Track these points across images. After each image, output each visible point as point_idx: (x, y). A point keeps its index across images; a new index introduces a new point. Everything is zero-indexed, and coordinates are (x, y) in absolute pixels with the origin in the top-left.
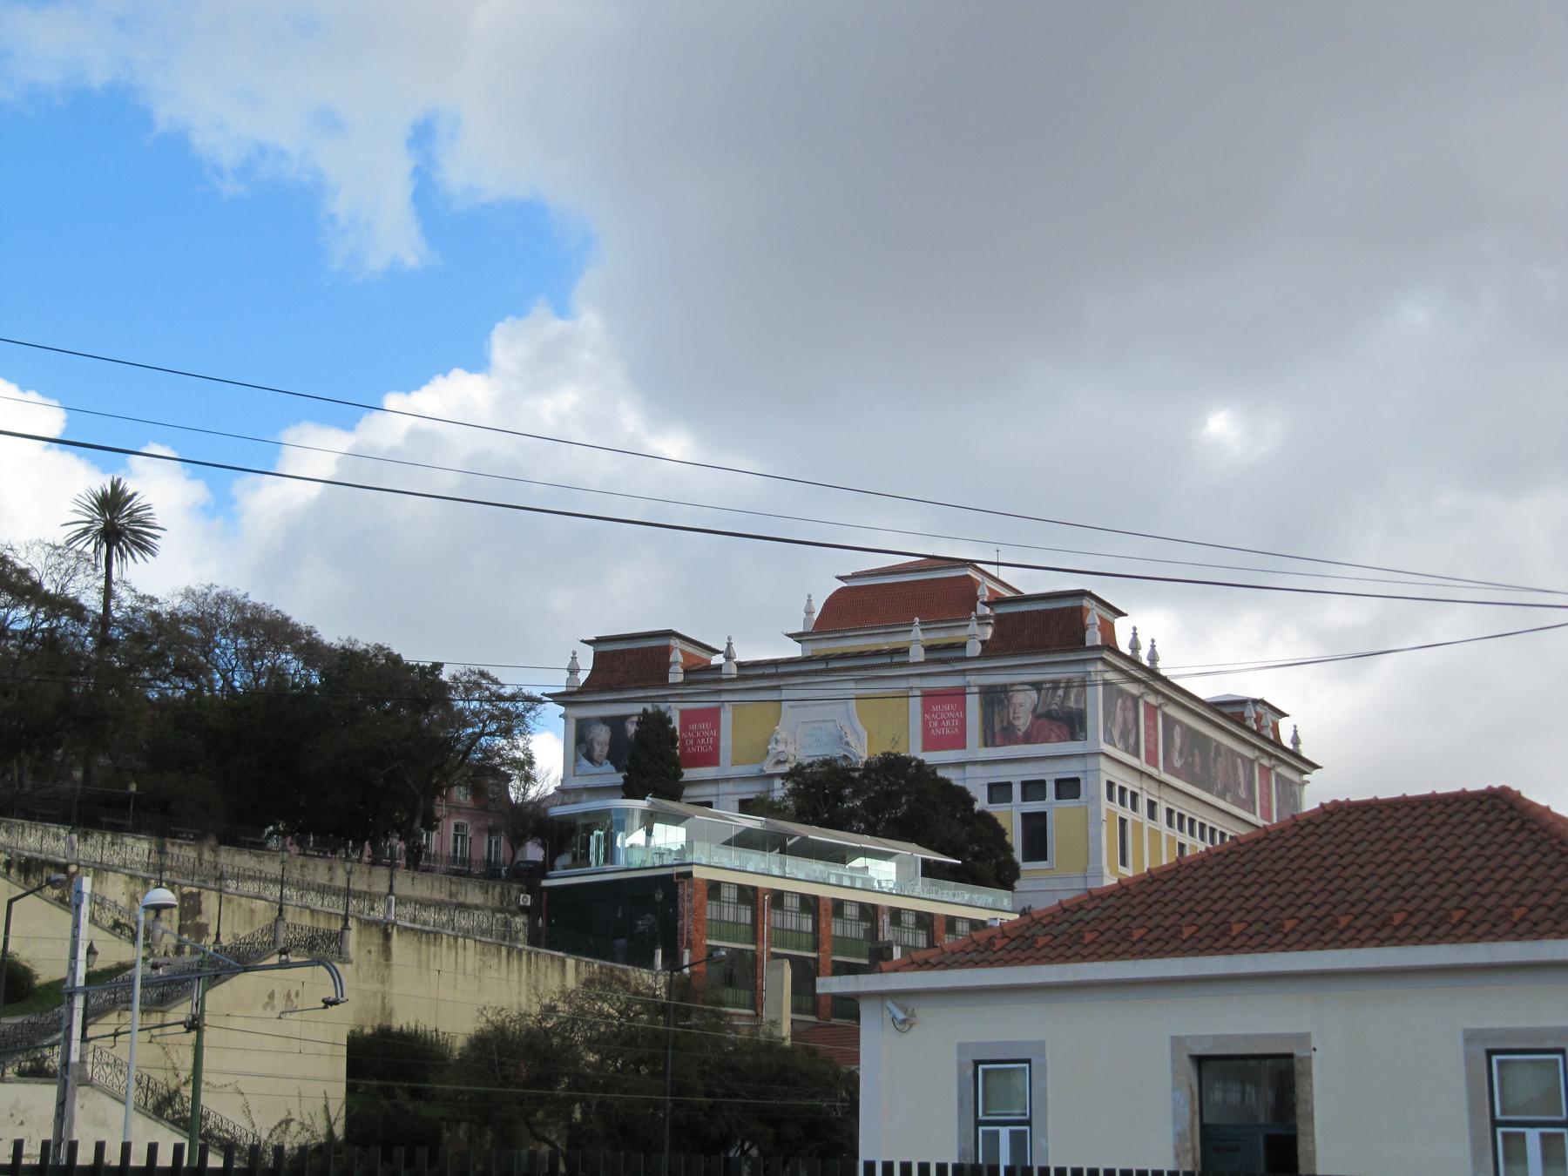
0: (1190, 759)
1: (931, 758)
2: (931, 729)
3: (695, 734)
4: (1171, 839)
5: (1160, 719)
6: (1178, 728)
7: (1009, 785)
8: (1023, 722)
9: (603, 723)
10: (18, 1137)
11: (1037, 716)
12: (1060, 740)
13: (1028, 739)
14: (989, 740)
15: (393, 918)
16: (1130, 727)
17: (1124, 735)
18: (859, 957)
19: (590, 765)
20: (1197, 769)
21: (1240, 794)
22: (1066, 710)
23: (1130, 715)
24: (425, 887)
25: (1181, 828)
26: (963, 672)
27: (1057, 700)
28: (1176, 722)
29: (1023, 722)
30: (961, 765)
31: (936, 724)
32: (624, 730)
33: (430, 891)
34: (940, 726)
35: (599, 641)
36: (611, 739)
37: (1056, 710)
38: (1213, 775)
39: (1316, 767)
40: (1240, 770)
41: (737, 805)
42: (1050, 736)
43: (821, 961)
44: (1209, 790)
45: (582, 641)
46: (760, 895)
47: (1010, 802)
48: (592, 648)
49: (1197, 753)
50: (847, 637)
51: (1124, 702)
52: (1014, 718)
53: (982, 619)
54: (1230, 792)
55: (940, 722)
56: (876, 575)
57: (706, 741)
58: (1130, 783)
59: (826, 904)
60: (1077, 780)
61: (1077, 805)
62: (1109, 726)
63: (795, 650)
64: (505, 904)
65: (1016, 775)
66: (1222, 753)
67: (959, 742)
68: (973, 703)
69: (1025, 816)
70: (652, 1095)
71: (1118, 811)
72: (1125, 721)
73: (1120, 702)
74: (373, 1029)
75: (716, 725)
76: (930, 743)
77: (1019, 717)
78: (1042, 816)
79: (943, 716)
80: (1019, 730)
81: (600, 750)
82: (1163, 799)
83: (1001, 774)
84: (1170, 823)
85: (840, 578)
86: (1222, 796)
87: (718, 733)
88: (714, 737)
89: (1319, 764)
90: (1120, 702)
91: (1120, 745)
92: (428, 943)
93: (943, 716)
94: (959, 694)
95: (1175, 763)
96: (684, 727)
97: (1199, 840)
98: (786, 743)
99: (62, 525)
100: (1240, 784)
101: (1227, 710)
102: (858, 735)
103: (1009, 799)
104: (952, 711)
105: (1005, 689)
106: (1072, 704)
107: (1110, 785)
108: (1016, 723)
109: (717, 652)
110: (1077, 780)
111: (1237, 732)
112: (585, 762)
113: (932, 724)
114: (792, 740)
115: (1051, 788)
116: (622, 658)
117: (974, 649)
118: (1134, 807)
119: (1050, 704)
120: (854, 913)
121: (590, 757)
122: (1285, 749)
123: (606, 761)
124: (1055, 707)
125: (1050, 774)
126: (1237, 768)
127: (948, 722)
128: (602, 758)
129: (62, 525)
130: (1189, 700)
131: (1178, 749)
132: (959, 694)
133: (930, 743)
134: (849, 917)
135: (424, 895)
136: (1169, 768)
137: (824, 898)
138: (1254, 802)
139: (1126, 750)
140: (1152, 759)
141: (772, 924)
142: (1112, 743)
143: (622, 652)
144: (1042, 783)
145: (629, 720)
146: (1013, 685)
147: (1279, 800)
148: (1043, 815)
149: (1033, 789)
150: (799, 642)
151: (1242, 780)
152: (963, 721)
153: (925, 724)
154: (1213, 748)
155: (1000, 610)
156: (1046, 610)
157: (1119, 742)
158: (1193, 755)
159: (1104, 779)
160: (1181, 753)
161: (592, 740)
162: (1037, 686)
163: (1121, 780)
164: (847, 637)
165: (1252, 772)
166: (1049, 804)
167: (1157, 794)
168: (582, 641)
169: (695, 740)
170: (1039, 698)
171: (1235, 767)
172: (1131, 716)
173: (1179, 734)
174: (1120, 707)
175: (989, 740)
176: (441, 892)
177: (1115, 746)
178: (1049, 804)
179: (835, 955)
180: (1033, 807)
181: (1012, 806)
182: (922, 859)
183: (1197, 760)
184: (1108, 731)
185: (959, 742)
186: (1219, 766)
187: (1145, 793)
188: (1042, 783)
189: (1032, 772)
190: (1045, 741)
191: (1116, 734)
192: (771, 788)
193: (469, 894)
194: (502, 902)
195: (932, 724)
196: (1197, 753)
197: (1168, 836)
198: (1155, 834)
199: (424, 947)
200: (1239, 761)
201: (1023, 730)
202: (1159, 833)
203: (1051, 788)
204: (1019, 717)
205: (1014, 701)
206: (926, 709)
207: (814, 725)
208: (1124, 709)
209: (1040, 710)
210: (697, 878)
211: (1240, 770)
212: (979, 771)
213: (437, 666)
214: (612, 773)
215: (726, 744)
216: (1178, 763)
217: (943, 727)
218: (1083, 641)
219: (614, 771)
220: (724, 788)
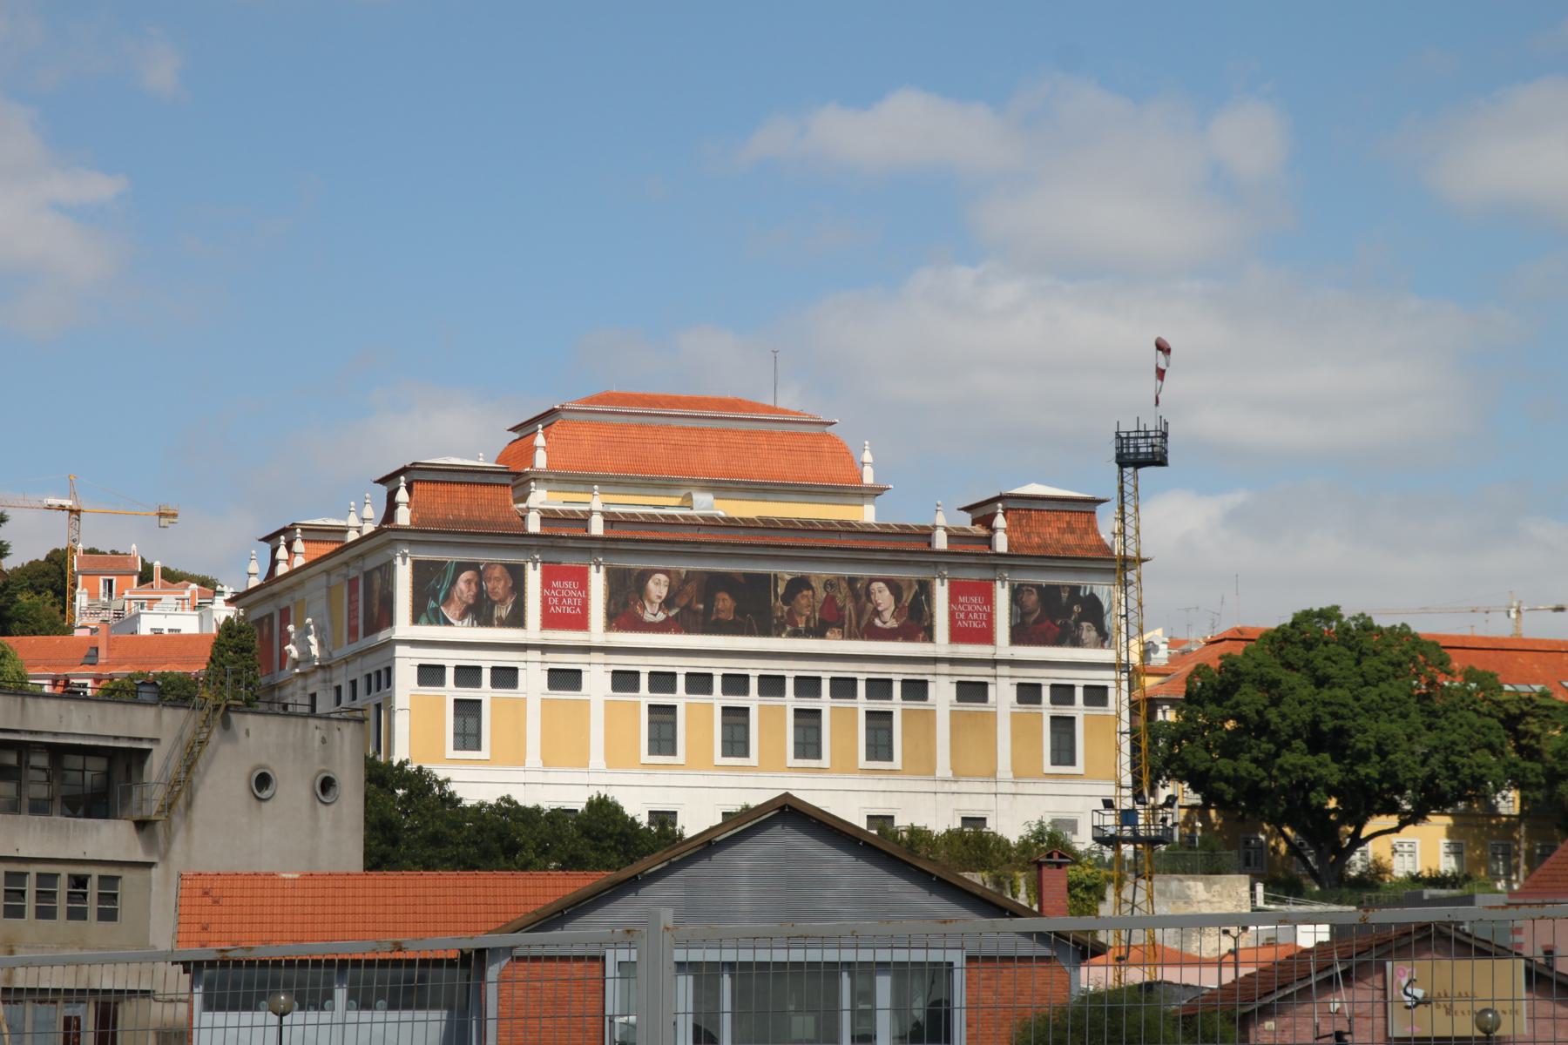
2: (550, 606)
3: (966, 608)
7: (479, 669)
10: (352, 679)
48: (269, 545)
50: (839, 493)
74: (1431, 874)
78: (476, 704)
79: (970, 608)
88: (988, 613)
93: (564, 593)
99: (1138, 418)
104: (979, 604)
113: (959, 616)
127: (570, 601)
129: (1138, 418)
153: (952, 614)
166: (485, 692)
178: (485, 692)
195: (552, 600)
217: (564, 605)
220: (1002, 670)
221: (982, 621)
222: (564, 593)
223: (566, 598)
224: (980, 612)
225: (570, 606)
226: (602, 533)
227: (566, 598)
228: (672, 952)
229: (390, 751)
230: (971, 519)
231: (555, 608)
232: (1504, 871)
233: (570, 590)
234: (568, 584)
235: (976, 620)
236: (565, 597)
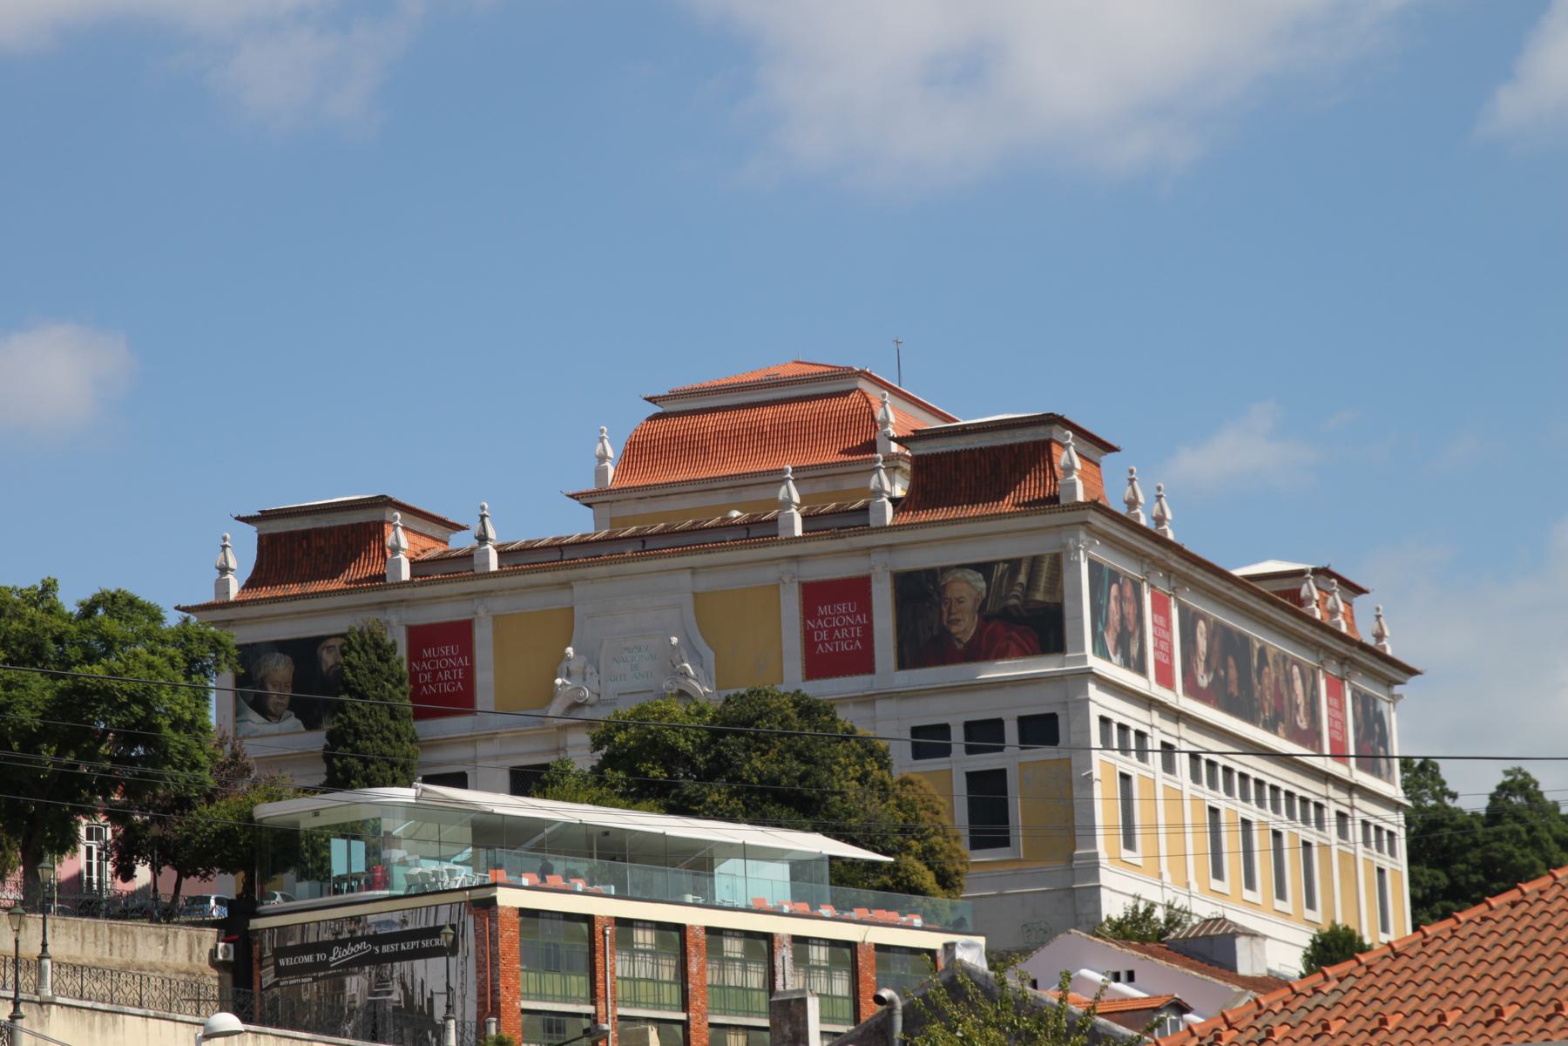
0: (1222, 673)
1: (822, 689)
2: (817, 643)
3: (433, 665)
4: (1293, 836)
5: (1348, 695)
6: (1201, 624)
8: (965, 627)
9: (280, 651)
14: (907, 659)
15: (50, 994)
16: (1130, 629)
17: (1123, 642)
18: (748, 1016)
19: (262, 719)
20: (1234, 689)
21: (1299, 723)
23: (1130, 609)
24: (73, 938)
25: (1276, 809)
26: (868, 551)
27: (1018, 590)
28: (1198, 616)
29: (965, 627)
30: (868, 700)
31: (824, 635)
32: (315, 661)
33: (79, 948)
35: (266, 516)
36: (294, 674)
37: (1015, 606)
38: (1257, 695)
39: (1412, 672)
40: (1298, 684)
41: (505, 777)
43: (692, 1024)
44: (1251, 718)
45: (238, 518)
46: (598, 927)
47: (948, 756)
49: (1231, 661)
51: (1120, 590)
52: (949, 622)
53: (892, 463)
54: (1283, 721)
55: (831, 632)
57: (452, 675)
58: (1136, 717)
59: (696, 936)
60: (1053, 718)
61: (1056, 756)
62: (1100, 628)
63: (580, 523)
64: (195, 958)
65: (955, 713)
66: (1270, 660)
67: (862, 662)
69: (973, 778)
71: (1118, 763)
72: (1123, 618)
73: (1114, 588)
75: (467, 649)
76: (817, 666)
77: (958, 620)
79: (836, 622)
80: (959, 640)
81: (277, 695)
82: (1156, 727)
83: (931, 713)
84: (1196, 777)
85: (649, 399)
86: (1271, 727)
87: (471, 660)
89: (1417, 667)
90: (1114, 588)
91: (1117, 659)
92: (103, 1030)
93: (836, 622)
95: (1200, 679)
96: (415, 654)
97: (1285, 818)
98: (584, 674)
100: (1297, 707)
101: (1263, 587)
102: (701, 656)
103: (945, 751)
106: (1039, 597)
107: (1105, 721)
108: (954, 629)
109: (457, 527)
110: (1053, 718)
111: (1241, 599)
112: (255, 717)
114: (594, 670)
115: (1011, 732)
116: (305, 545)
118: (1320, 824)
120: (823, 957)
121: (260, 706)
122: (1363, 647)
123: (288, 712)
124: (1013, 601)
125: (1009, 710)
126: (1292, 681)
127: (447, 675)
128: (280, 708)
130: (1125, 530)
131: (1203, 658)
133: (817, 666)
134: (641, 947)
135: (72, 952)
136: (1192, 690)
137: (692, 927)
138: (1319, 735)
139: (1127, 664)
140: (1165, 678)
141: (618, 973)
142: (1103, 653)
143: (306, 535)
144: (998, 724)
145: (324, 644)
146: (945, 569)
147: (1357, 729)
148: (1001, 773)
149: (985, 734)
150: (589, 505)
151: (1300, 700)
152: (868, 630)
153: (808, 635)
154: (1256, 653)
155: (924, 448)
156: (993, 449)
157: (1115, 654)
158: (1226, 667)
159: (1095, 713)
160: (1207, 662)
161: (262, 679)
162: (984, 568)
164: (667, 495)
165: (1315, 687)
166: (1011, 758)
167: (1347, 801)
168: (238, 518)
169: (434, 673)
170: (988, 589)
171: (1289, 681)
172: (1131, 612)
173: (1205, 635)
174: (1116, 598)
175: (907, 659)
176: (96, 946)
177: (1109, 659)
178: (1011, 758)
179: (714, 1014)
180: (986, 762)
181: (950, 762)
183: (1233, 673)
184: (1098, 638)
185: (862, 662)
186: (1266, 681)
187: (1156, 731)
188: (998, 724)
189: (982, 708)
190: (1002, 654)
191: (1110, 642)
192: (561, 745)
193: (139, 946)
194: (190, 958)
196: (1231, 661)
197: (1194, 799)
198: (1175, 797)
199: (97, 1034)
200: (1296, 669)
201: (967, 639)
202: (1329, 847)
203: (1011, 732)
204: (958, 620)
205: (948, 595)
206: (809, 611)
208: (1121, 598)
210: (503, 907)
211: (1298, 684)
213: (48, 587)
214: (300, 732)
215: (484, 678)
216: (1203, 681)
219: (302, 728)
220: (484, 749)
221: (854, 639)
222: (439, 664)
223: (839, 629)
224: (851, 625)
225: (845, 639)
226: (592, 530)
227: (839, 629)
228: (1377, 950)
229: (714, 898)
230: (256, 536)
231: (824, 646)
232: (254, 947)
233: (844, 615)
234: (841, 608)
235: (448, 680)
236: (440, 669)
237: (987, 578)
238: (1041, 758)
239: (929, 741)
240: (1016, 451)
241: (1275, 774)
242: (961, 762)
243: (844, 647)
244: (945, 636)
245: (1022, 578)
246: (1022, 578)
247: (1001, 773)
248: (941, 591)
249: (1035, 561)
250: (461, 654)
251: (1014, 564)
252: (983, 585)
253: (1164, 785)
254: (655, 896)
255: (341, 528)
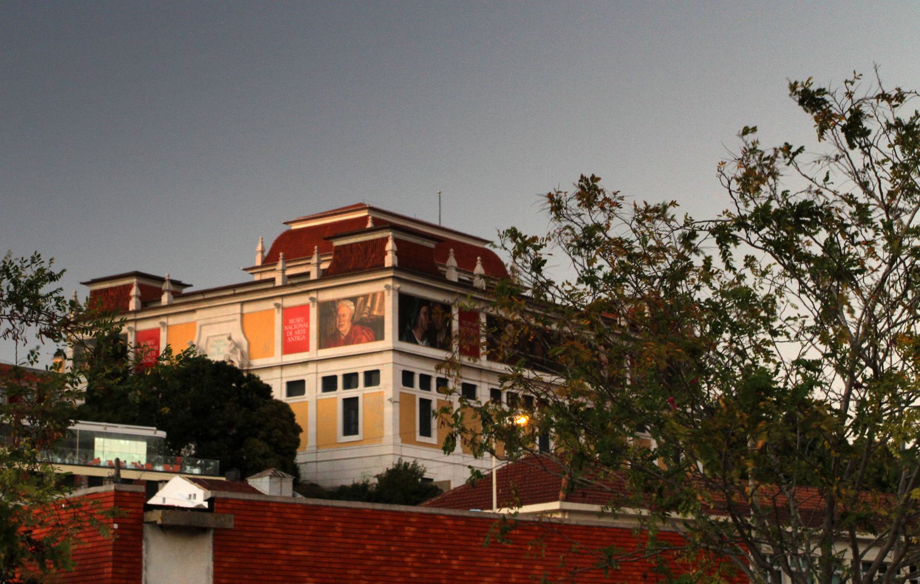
8: (345, 328)
11: (354, 323)
12: (369, 341)
13: (349, 341)
22: (372, 317)
27: (367, 310)
29: (345, 328)
34: (294, 335)
42: (362, 339)
55: (294, 331)
56: (332, 215)
65: (338, 369)
68: (313, 313)
70: (468, 507)
79: (296, 327)
93: (296, 327)
94: (303, 311)
105: (333, 303)
106: (375, 313)
108: (341, 329)
117: (314, 276)
119: (362, 314)
124: (365, 316)
125: (360, 367)
132: (303, 311)
143: (106, 291)
146: (339, 300)
148: (356, 399)
149: (350, 380)
152: (308, 330)
162: (354, 299)
163: (420, 369)
169: (294, 331)
170: (355, 310)
178: (360, 391)
180: (351, 393)
182: (438, 400)
190: (359, 342)
201: (346, 334)
207: (217, 338)
209: (356, 319)
212: (276, 373)
218: (383, 264)
237: (355, 304)
238: (372, 391)
239: (329, 383)
240: (137, 560)
241: (369, 358)
242: (342, 393)
243: (298, 339)
244: (337, 333)
245: (369, 304)
246: (369, 304)
247: (356, 399)
248: (337, 311)
249: (374, 295)
250: (155, 345)
251: (366, 297)
252: (353, 308)
253: (400, 393)
254: (180, 512)
255: (120, 287)
